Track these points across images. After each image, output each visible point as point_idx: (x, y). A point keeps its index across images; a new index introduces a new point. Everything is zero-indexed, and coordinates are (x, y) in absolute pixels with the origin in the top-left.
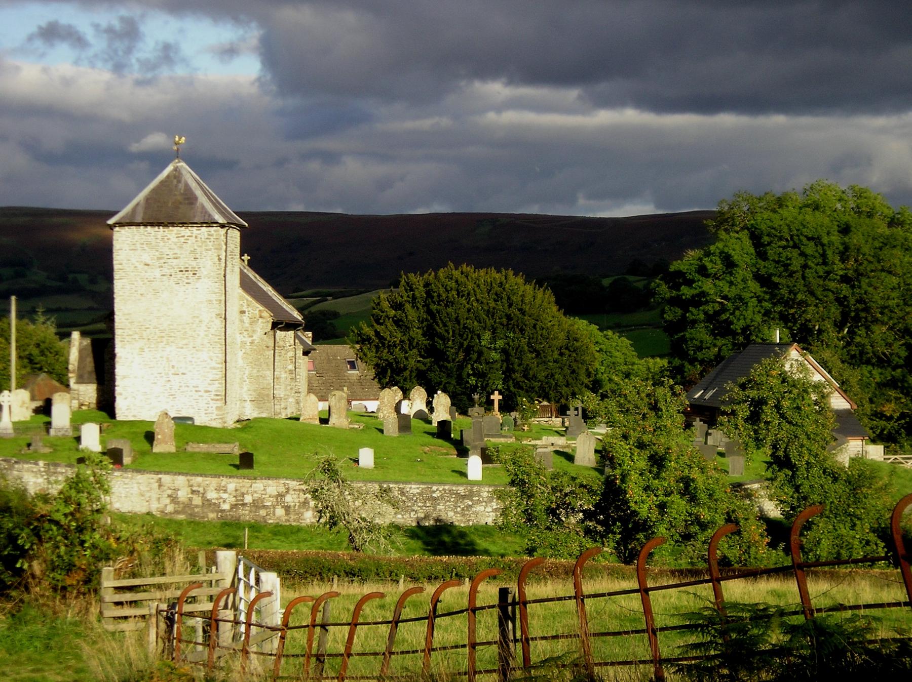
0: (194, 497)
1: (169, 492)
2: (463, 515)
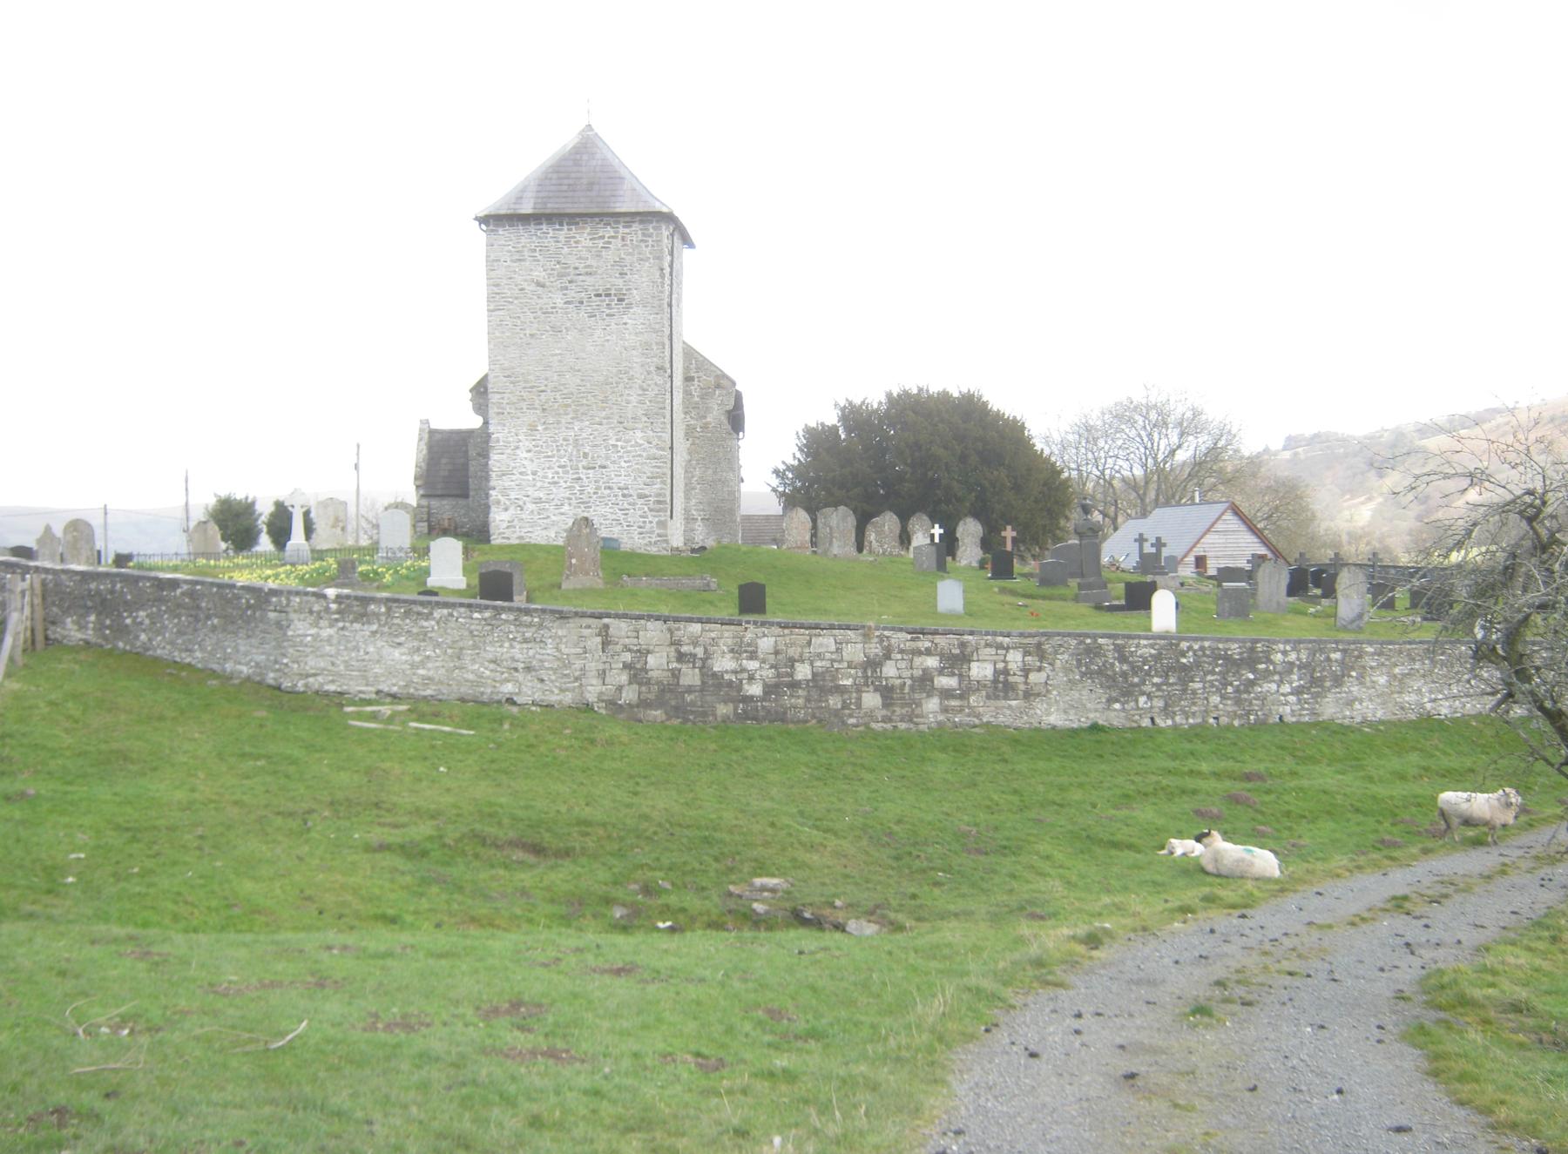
0: (685, 668)
1: (627, 657)
2: (1238, 702)
